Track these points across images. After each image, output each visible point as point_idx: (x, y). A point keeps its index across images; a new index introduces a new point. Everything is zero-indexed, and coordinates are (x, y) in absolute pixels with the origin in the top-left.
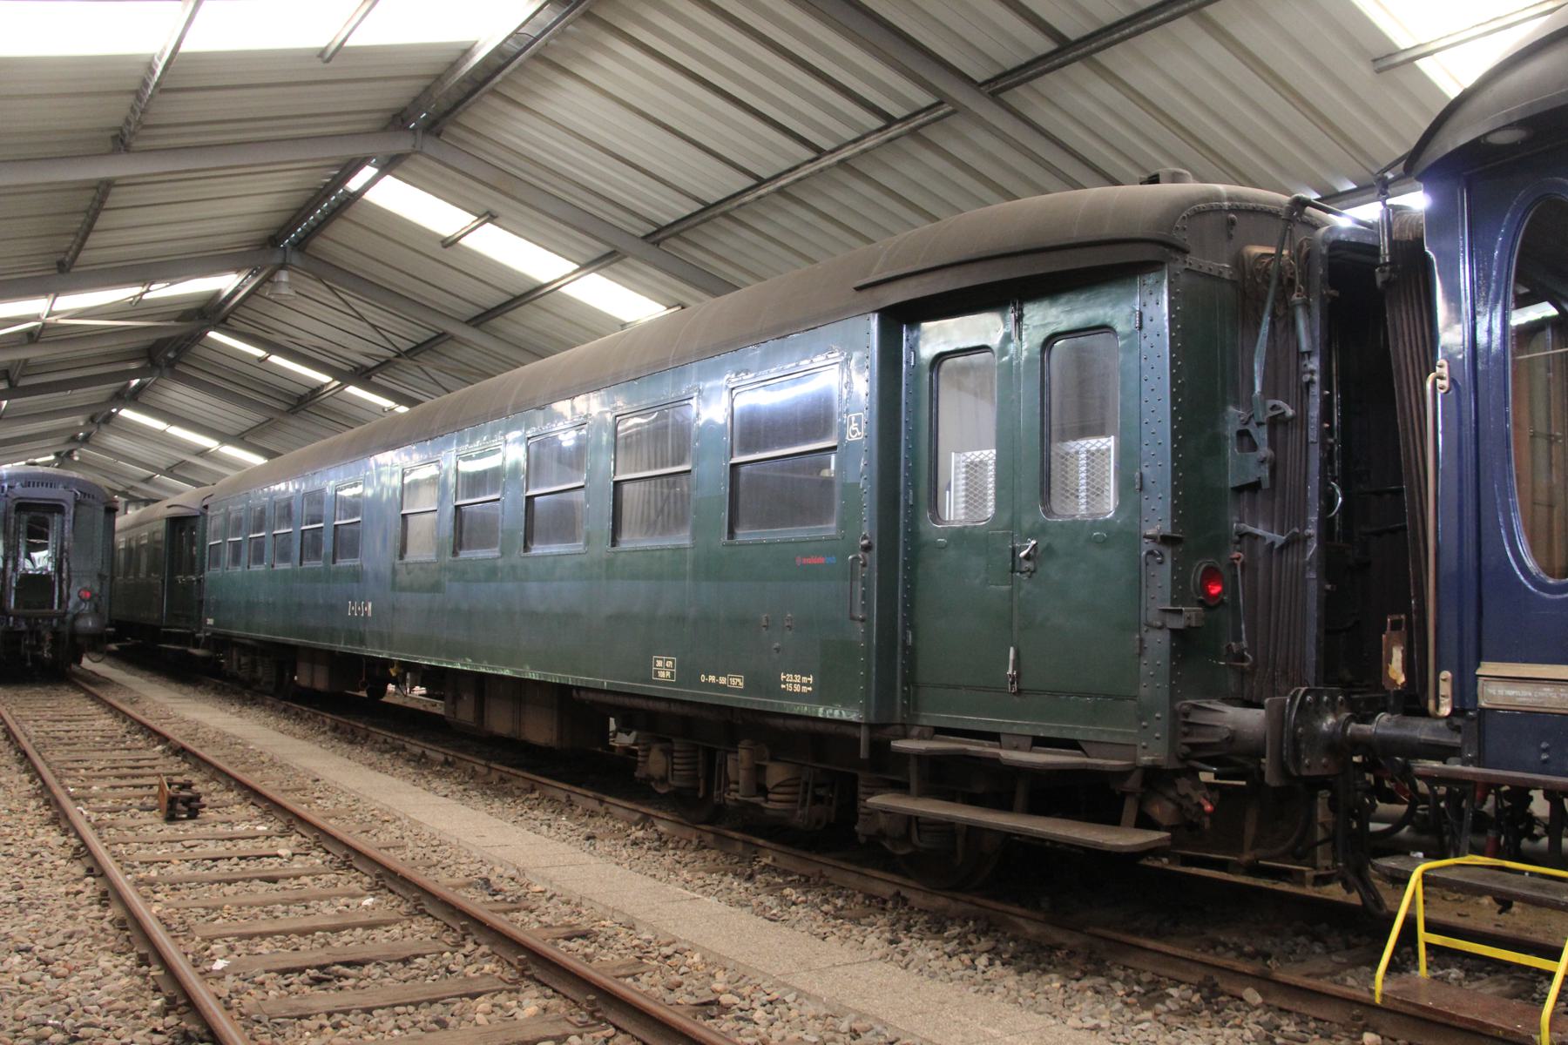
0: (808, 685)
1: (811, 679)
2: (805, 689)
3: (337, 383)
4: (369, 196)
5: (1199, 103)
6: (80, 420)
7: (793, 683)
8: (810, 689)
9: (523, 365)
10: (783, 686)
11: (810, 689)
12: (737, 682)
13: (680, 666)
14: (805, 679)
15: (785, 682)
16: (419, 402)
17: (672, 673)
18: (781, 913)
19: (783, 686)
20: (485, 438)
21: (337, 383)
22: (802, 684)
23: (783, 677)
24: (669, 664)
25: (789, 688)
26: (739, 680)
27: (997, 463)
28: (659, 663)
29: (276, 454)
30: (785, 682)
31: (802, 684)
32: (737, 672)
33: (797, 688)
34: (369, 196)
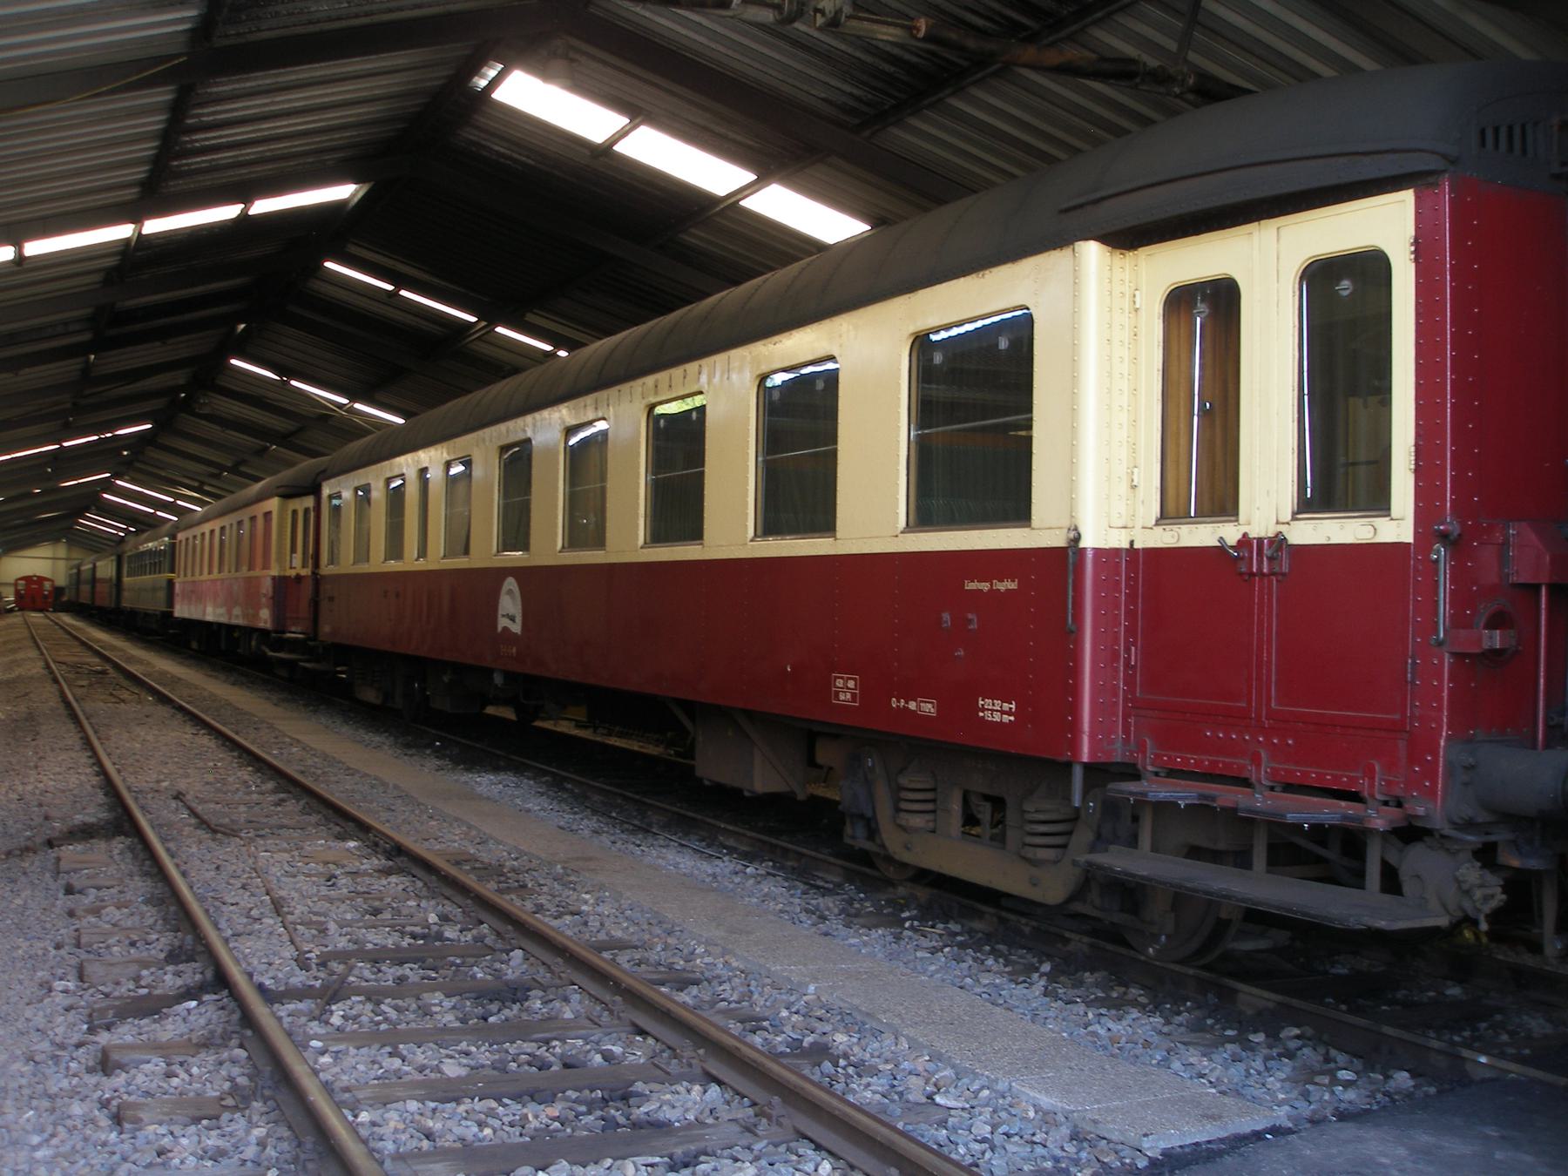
0: (1009, 713)
1: (1013, 706)
2: (1006, 718)
3: (483, 324)
4: (499, 95)
5: (547, 318)
6: (180, 377)
7: (992, 710)
8: (1012, 718)
9: (772, 269)
10: (981, 714)
11: (1012, 718)
12: (928, 708)
13: (864, 687)
14: (1006, 706)
15: (983, 710)
16: (582, 345)
17: (854, 695)
18: (931, 1066)
19: (981, 714)
20: (235, 587)
21: (483, 324)
22: (1003, 712)
23: (981, 702)
24: (851, 684)
25: (988, 716)
26: (930, 706)
27: (1423, 249)
28: (840, 683)
29: (415, 414)
30: (983, 710)
31: (1003, 712)
32: (928, 695)
33: (997, 717)
34: (499, 95)
